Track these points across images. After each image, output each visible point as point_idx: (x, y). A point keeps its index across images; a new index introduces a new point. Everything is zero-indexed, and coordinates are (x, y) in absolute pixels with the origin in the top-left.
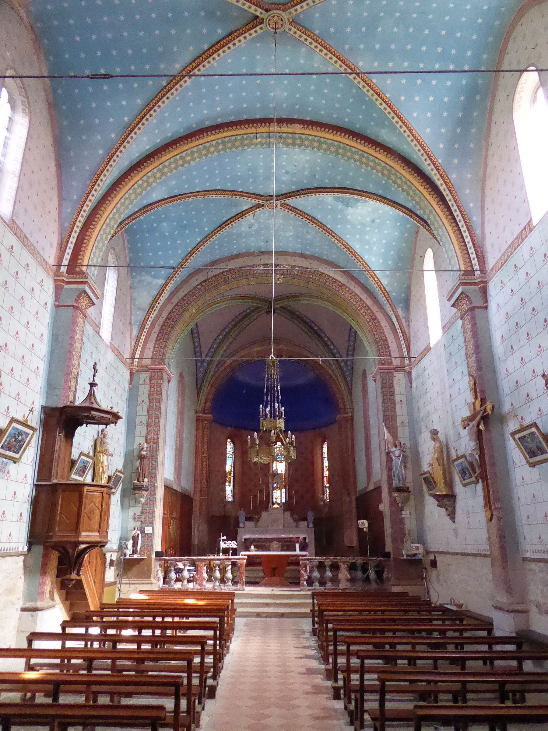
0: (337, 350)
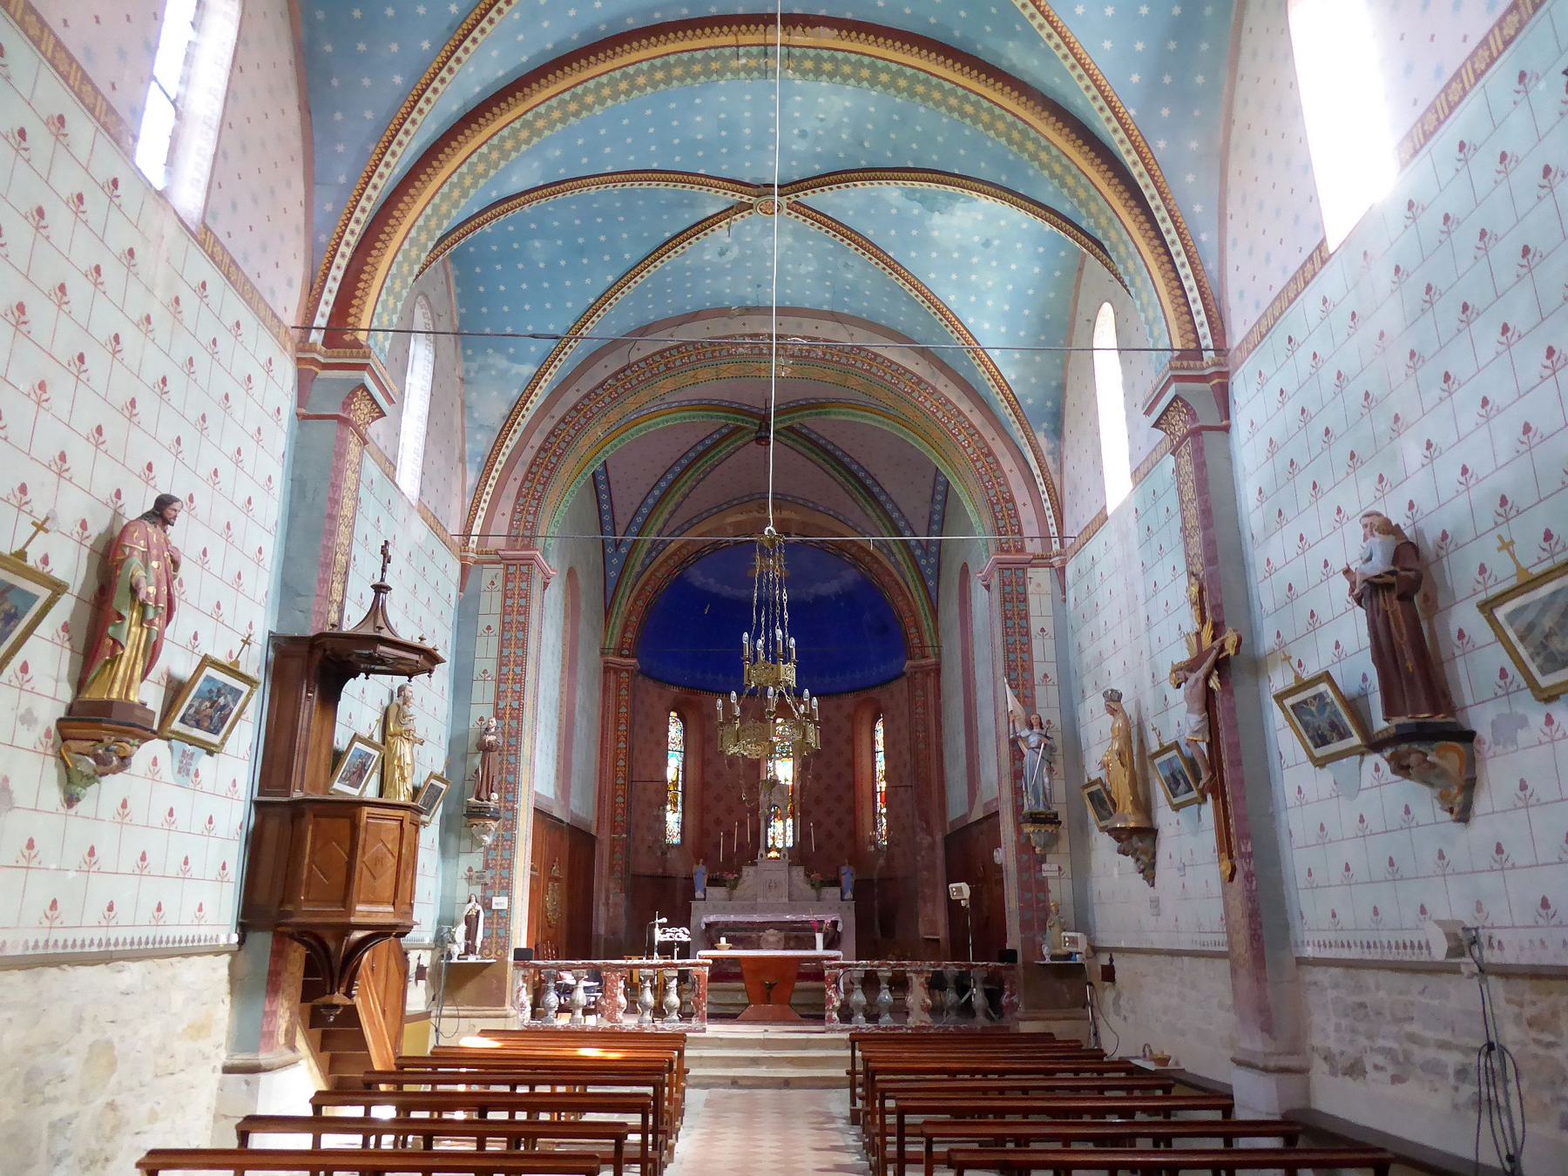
0: (907, 522)
